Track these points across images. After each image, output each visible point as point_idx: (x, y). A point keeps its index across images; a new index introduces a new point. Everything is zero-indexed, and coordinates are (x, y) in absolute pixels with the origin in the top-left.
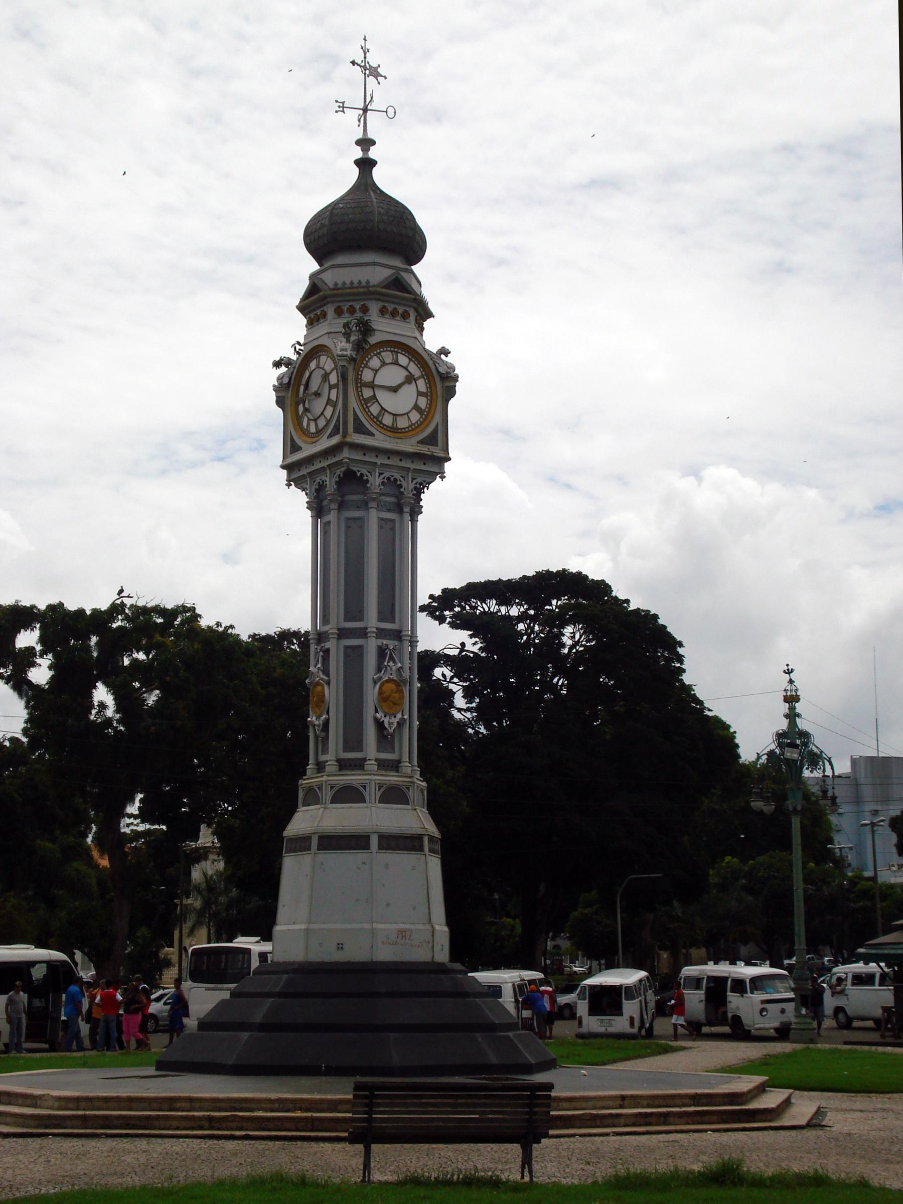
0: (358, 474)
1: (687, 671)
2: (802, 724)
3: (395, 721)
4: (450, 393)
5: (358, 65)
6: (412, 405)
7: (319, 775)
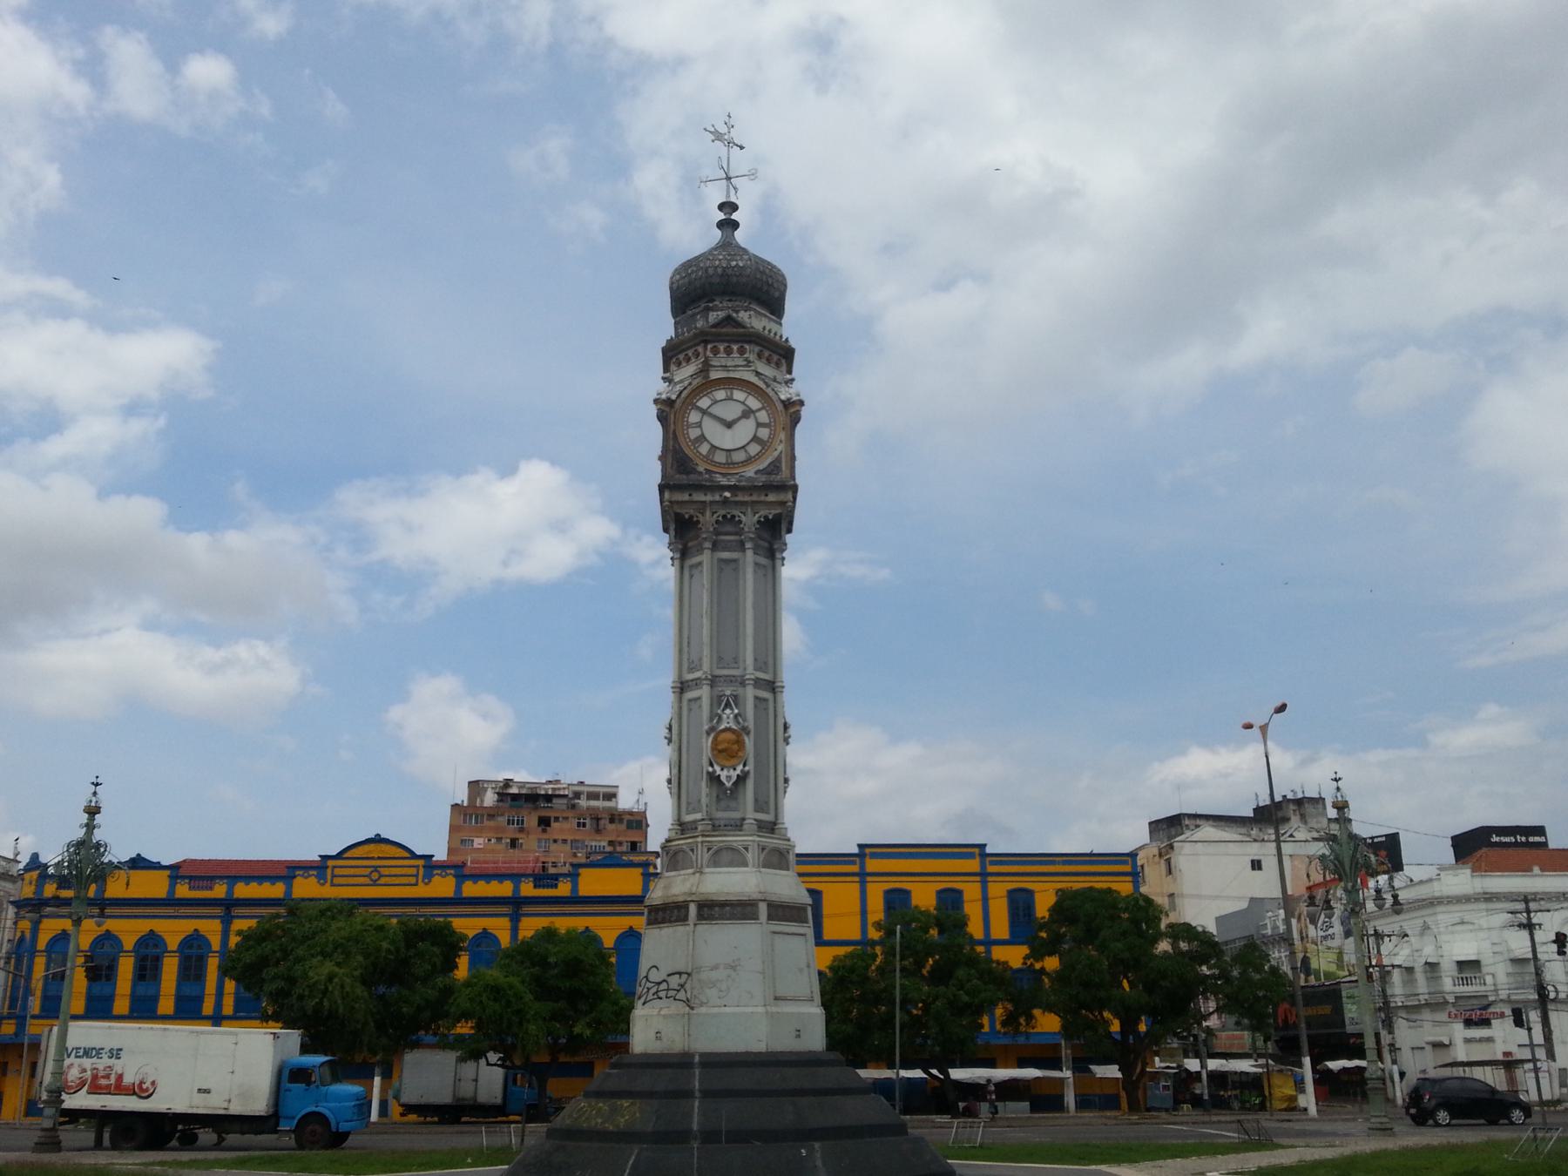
0: (687, 516)
1: (1286, 702)
2: (98, 835)
3: (734, 774)
4: (795, 420)
5: (737, 145)
6: (707, 436)
7: (682, 836)
